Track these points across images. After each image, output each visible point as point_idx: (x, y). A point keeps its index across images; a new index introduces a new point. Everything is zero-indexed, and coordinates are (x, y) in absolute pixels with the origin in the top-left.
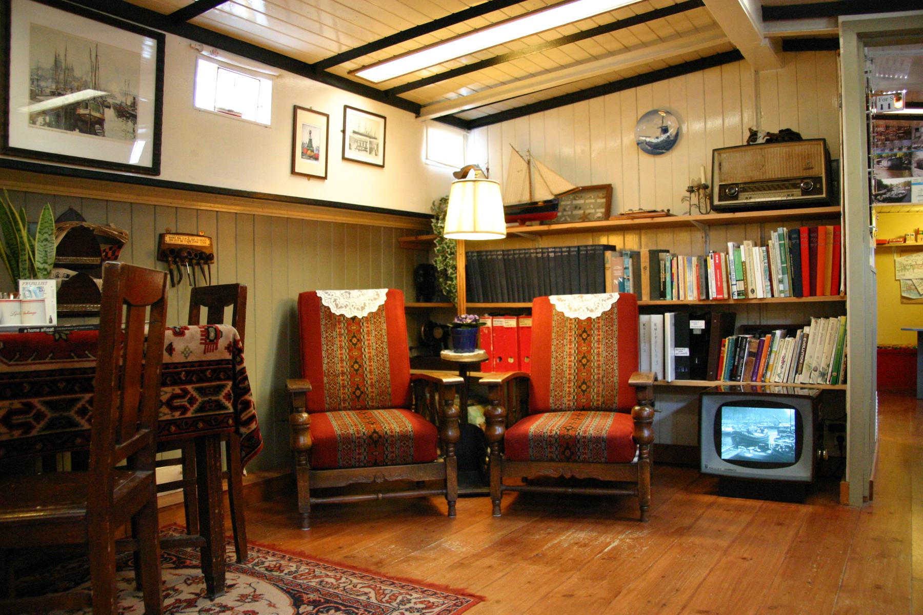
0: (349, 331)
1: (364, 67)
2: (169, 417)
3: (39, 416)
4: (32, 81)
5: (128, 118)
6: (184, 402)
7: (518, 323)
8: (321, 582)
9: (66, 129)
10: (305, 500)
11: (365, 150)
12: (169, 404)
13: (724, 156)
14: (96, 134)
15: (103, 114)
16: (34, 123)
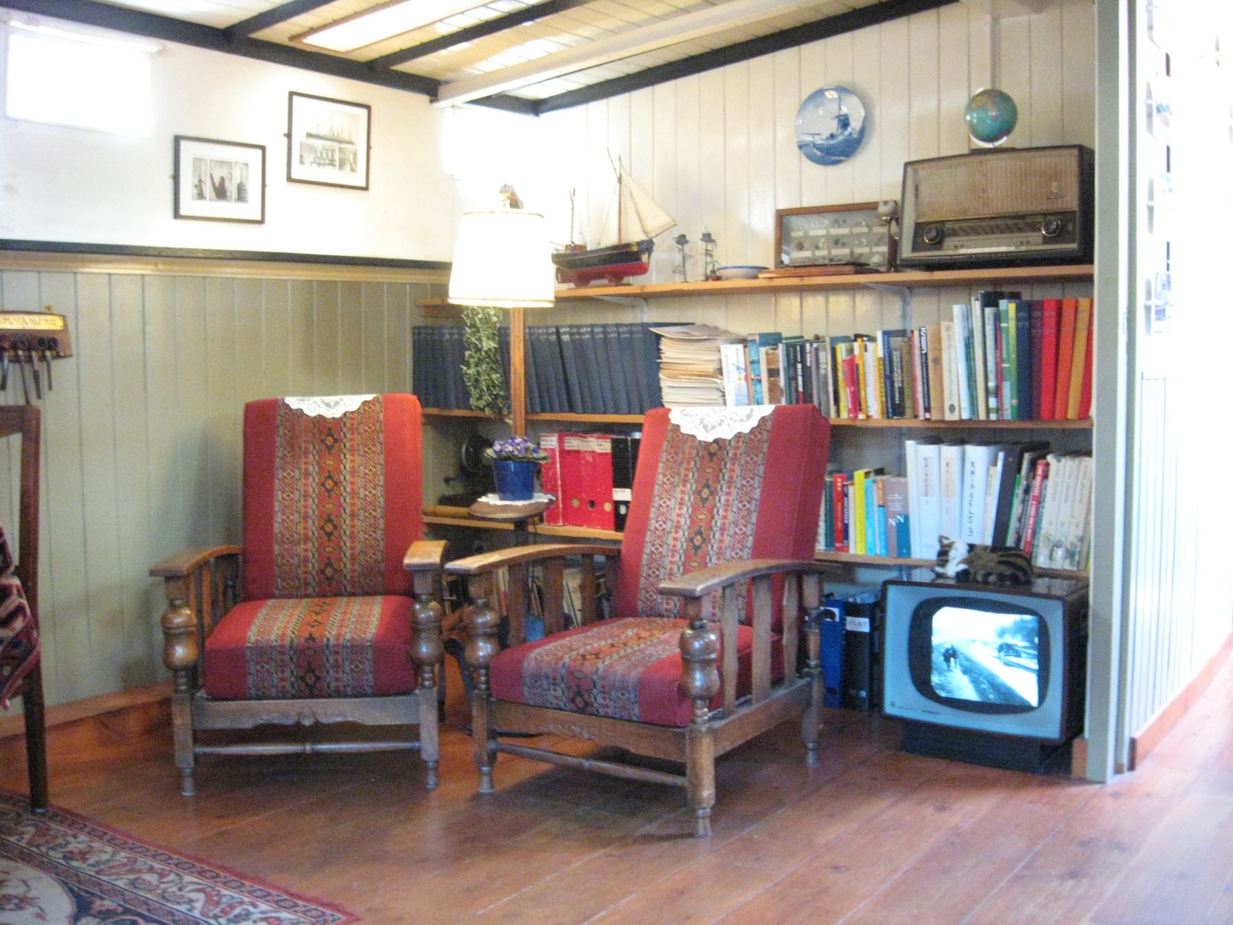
0: (321, 468)
1: (312, 31)
7: (561, 442)
8: (136, 879)
10: (185, 753)
11: (332, 163)
13: (922, 173)
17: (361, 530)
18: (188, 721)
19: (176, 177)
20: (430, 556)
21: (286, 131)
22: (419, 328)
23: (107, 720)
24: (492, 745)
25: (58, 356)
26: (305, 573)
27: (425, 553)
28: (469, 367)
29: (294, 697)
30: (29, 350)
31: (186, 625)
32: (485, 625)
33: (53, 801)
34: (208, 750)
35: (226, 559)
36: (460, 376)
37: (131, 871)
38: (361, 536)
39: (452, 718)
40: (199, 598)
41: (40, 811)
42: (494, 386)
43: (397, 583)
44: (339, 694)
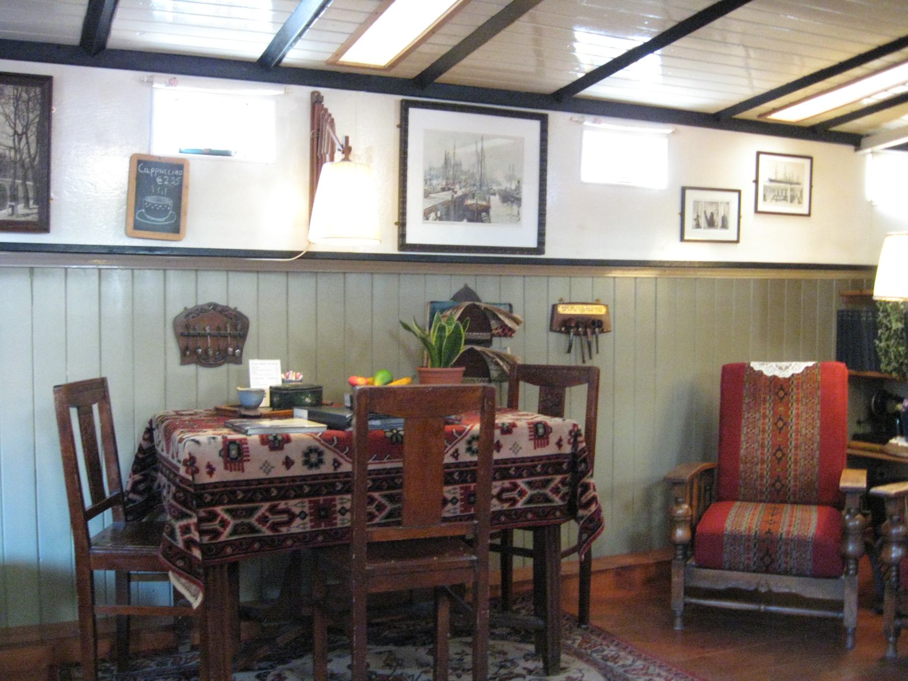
1: (775, 110)
2: (498, 508)
3: (522, 493)
4: (426, 181)
5: (512, 202)
6: (514, 494)
9: (455, 220)
10: (678, 602)
11: (785, 199)
12: (499, 497)
14: (482, 221)
15: (489, 202)
16: (427, 219)
17: (803, 457)
18: (681, 579)
19: (682, 214)
20: (858, 481)
21: (754, 178)
22: (842, 311)
23: (622, 572)
24: (898, 623)
25: (602, 331)
26: (761, 485)
27: (854, 479)
28: (881, 342)
29: (754, 571)
30: (586, 327)
31: (685, 516)
32: (898, 535)
33: (591, 621)
34: (694, 601)
35: (708, 472)
36: (874, 350)
37: (646, 674)
38: (802, 462)
39: (870, 601)
40: (691, 497)
41: (584, 626)
42: (900, 356)
43: (836, 499)
44: (786, 572)
